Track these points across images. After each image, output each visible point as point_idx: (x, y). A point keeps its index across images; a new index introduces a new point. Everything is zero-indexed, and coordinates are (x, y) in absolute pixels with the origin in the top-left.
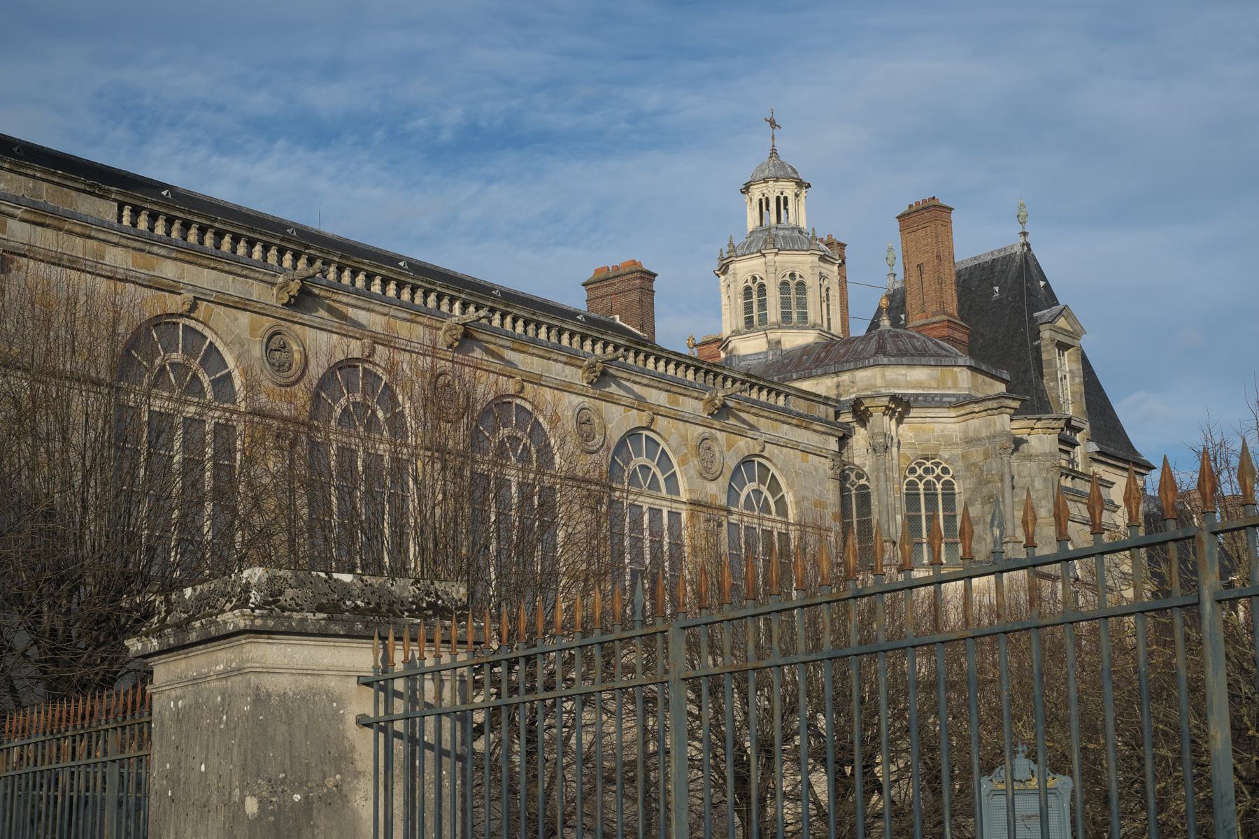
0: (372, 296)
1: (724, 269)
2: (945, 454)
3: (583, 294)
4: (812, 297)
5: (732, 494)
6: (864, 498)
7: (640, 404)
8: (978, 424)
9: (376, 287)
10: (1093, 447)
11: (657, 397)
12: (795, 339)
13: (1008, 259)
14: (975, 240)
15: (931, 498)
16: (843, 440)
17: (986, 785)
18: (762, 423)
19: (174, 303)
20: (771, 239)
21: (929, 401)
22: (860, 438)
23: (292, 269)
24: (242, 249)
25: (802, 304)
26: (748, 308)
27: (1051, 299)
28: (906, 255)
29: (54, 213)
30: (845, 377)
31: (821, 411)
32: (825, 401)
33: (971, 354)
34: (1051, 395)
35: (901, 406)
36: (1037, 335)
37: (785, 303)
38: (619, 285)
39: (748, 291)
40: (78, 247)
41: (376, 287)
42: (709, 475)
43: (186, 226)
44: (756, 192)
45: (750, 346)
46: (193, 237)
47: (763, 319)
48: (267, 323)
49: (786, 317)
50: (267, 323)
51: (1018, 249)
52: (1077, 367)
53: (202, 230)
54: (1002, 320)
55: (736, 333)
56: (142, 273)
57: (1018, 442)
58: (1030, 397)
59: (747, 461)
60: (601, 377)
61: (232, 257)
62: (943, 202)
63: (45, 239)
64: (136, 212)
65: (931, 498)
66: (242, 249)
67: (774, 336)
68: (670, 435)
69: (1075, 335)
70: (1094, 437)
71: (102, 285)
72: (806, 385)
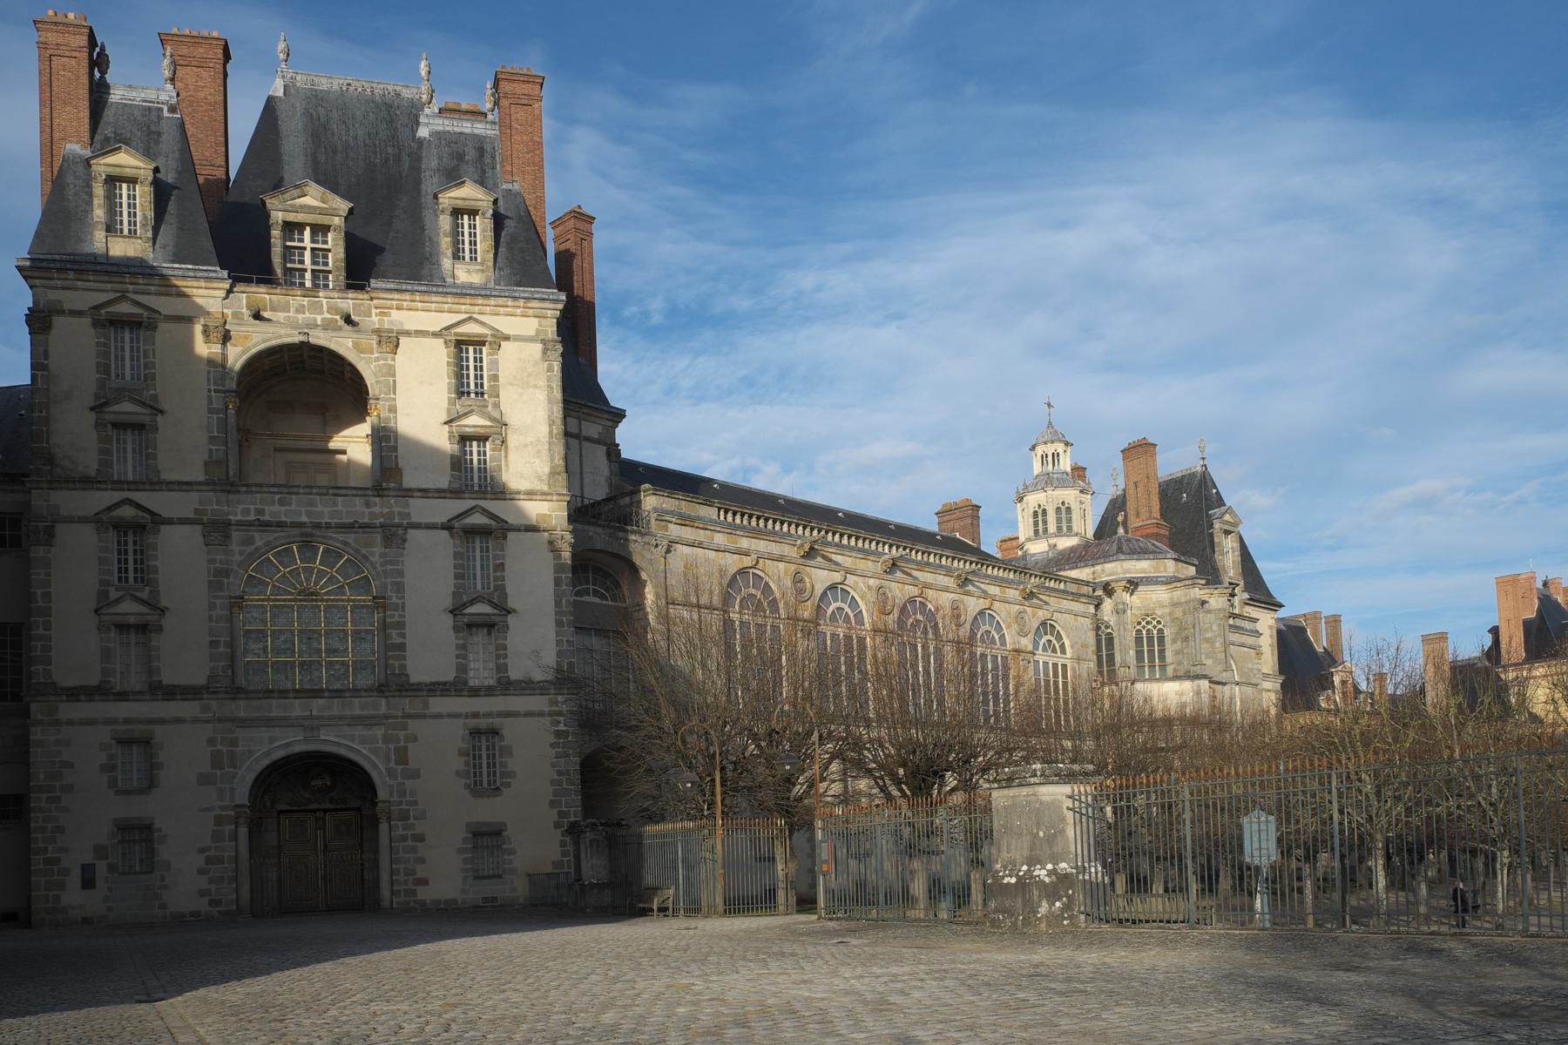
0: (843, 546)
1: (1021, 500)
2: (1159, 612)
3: (936, 519)
4: (1075, 516)
5: (1036, 644)
6: (1110, 640)
7: (985, 595)
8: (1179, 594)
9: (845, 541)
10: (1246, 596)
11: (994, 590)
12: (1065, 543)
13: (1192, 475)
14: (1171, 463)
15: (1150, 639)
16: (1097, 607)
17: (1245, 820)
18: (1051, 600)
19: (747, 561)
20: (1048, 481)
21: (1149, 581)
22: (1108, 604)
23: (809, 535)
24: (778, 527)
25: (1069, 520)
26: (1036, 524)
27: (1220, 502)
28: (1126, 476)
29: (689, 518)
30: (1098, 568)
31: (1085, 590)
32: (1087, 583)
33: (1172, 547)
34: (1219, 564)
35: (1133, 585)
36: (1211, 526)
37: (1059, 520)
38: (958, 514)
39: (1035, 513)
40: (701, 535)
41: (845, 541)
42: (1022, 633)
43: (750, 516)
44: (1040, 450)
45: (1038, 548)
46: (754, 522)
47: (1045, 530)
48: (793, 567)
49: (1059, 529)
50: (793, 567)
51: (1199, 469)
52: (1237, 545)
53: (758, 518)
54: (1186, 517)
55: (1029, 540)
56: (732, 546)
57: (1203, 603)
58: (1210, 574)
59: (1044, 624)
60: (964, 582)
61: (774, 533)
62: (1151, 440)
63: (688, 533)
64: (726, 512)
65: (1150, 639)
66: (778, 527)
67: (1052, 541)
68: (1003, 612)
69: (1235, 525)
70: (1246, 589)
71: (712, 554)
72: (1074, 574)
